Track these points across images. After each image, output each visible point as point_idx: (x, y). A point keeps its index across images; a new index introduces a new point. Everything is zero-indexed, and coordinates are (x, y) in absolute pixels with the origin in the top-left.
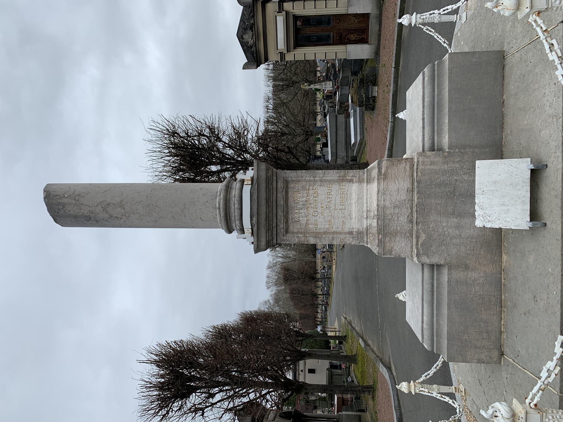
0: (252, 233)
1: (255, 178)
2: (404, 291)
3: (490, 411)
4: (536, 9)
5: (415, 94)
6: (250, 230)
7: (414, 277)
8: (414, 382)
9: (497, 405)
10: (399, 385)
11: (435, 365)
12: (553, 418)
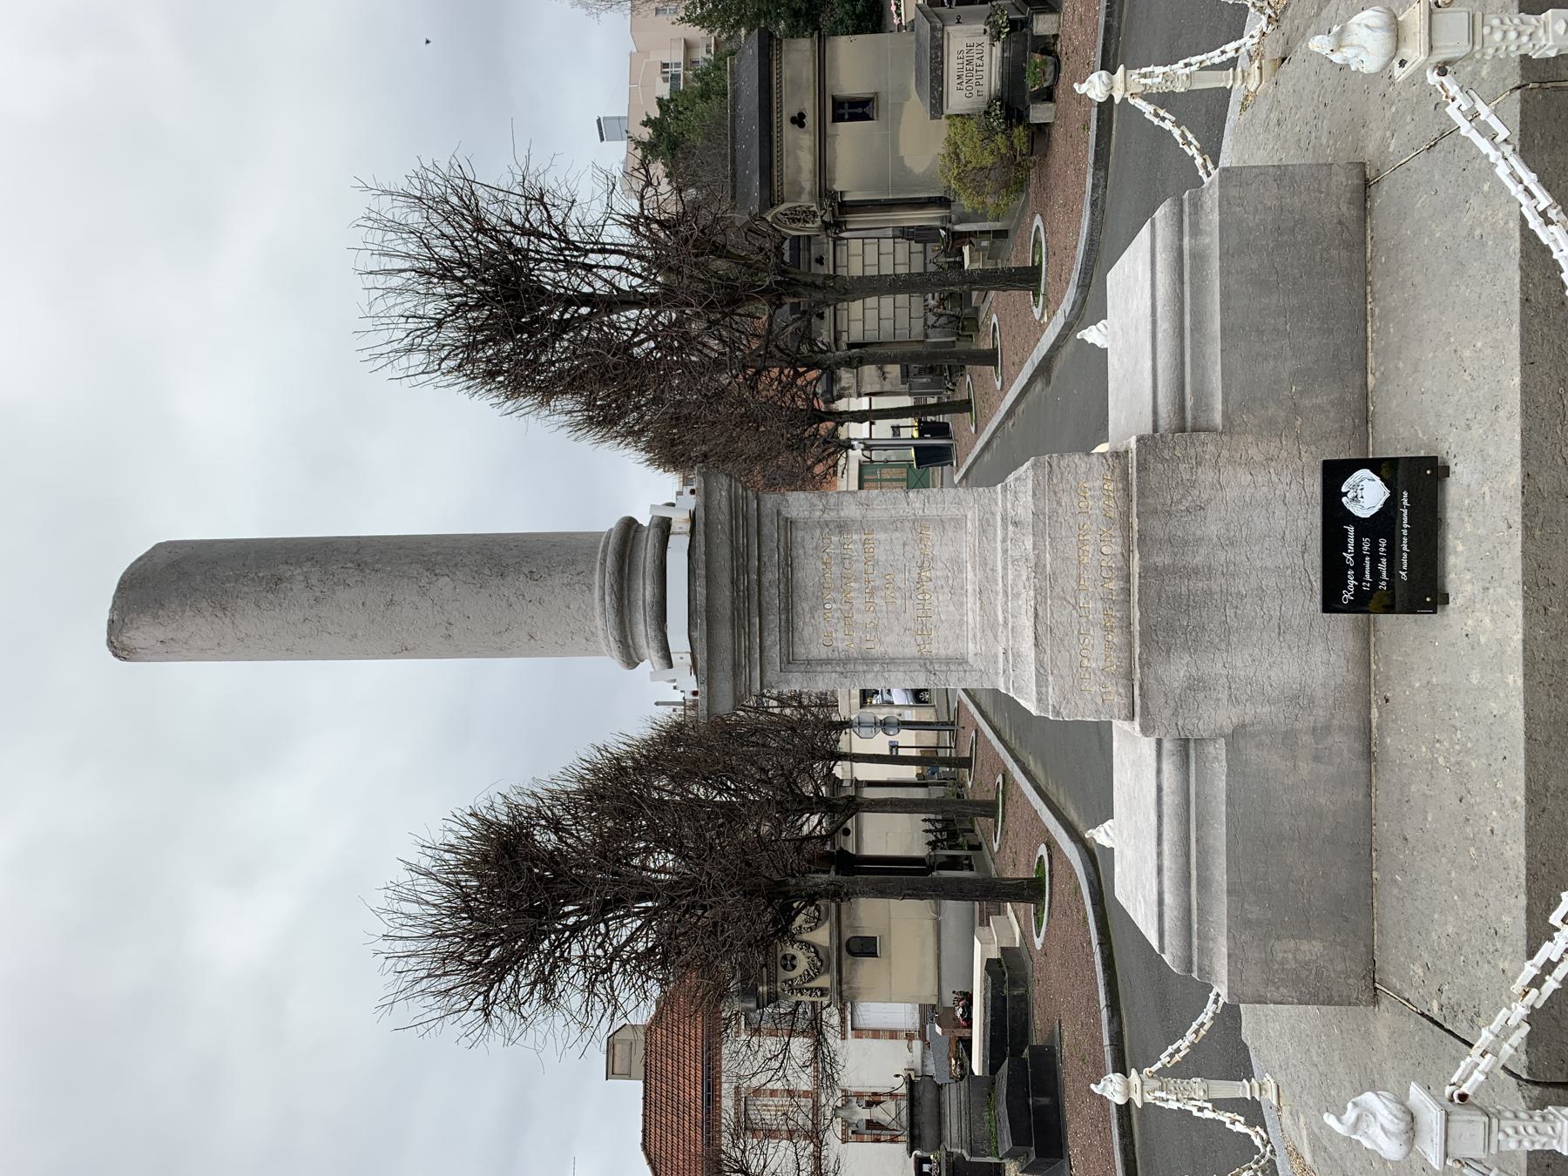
0: (694, 665)
1: (701, 514)
2: (1110, 822)
3: (1351, 1115)
4: (1440, 56)
5: (1135, 279)
6: (688, 659)
7: (1135, 764)
8: (1139, 1072)
9: (1368, 1097)
10: (1098, 1083)
11: (1195, 1026)
12: (1517, 1132)
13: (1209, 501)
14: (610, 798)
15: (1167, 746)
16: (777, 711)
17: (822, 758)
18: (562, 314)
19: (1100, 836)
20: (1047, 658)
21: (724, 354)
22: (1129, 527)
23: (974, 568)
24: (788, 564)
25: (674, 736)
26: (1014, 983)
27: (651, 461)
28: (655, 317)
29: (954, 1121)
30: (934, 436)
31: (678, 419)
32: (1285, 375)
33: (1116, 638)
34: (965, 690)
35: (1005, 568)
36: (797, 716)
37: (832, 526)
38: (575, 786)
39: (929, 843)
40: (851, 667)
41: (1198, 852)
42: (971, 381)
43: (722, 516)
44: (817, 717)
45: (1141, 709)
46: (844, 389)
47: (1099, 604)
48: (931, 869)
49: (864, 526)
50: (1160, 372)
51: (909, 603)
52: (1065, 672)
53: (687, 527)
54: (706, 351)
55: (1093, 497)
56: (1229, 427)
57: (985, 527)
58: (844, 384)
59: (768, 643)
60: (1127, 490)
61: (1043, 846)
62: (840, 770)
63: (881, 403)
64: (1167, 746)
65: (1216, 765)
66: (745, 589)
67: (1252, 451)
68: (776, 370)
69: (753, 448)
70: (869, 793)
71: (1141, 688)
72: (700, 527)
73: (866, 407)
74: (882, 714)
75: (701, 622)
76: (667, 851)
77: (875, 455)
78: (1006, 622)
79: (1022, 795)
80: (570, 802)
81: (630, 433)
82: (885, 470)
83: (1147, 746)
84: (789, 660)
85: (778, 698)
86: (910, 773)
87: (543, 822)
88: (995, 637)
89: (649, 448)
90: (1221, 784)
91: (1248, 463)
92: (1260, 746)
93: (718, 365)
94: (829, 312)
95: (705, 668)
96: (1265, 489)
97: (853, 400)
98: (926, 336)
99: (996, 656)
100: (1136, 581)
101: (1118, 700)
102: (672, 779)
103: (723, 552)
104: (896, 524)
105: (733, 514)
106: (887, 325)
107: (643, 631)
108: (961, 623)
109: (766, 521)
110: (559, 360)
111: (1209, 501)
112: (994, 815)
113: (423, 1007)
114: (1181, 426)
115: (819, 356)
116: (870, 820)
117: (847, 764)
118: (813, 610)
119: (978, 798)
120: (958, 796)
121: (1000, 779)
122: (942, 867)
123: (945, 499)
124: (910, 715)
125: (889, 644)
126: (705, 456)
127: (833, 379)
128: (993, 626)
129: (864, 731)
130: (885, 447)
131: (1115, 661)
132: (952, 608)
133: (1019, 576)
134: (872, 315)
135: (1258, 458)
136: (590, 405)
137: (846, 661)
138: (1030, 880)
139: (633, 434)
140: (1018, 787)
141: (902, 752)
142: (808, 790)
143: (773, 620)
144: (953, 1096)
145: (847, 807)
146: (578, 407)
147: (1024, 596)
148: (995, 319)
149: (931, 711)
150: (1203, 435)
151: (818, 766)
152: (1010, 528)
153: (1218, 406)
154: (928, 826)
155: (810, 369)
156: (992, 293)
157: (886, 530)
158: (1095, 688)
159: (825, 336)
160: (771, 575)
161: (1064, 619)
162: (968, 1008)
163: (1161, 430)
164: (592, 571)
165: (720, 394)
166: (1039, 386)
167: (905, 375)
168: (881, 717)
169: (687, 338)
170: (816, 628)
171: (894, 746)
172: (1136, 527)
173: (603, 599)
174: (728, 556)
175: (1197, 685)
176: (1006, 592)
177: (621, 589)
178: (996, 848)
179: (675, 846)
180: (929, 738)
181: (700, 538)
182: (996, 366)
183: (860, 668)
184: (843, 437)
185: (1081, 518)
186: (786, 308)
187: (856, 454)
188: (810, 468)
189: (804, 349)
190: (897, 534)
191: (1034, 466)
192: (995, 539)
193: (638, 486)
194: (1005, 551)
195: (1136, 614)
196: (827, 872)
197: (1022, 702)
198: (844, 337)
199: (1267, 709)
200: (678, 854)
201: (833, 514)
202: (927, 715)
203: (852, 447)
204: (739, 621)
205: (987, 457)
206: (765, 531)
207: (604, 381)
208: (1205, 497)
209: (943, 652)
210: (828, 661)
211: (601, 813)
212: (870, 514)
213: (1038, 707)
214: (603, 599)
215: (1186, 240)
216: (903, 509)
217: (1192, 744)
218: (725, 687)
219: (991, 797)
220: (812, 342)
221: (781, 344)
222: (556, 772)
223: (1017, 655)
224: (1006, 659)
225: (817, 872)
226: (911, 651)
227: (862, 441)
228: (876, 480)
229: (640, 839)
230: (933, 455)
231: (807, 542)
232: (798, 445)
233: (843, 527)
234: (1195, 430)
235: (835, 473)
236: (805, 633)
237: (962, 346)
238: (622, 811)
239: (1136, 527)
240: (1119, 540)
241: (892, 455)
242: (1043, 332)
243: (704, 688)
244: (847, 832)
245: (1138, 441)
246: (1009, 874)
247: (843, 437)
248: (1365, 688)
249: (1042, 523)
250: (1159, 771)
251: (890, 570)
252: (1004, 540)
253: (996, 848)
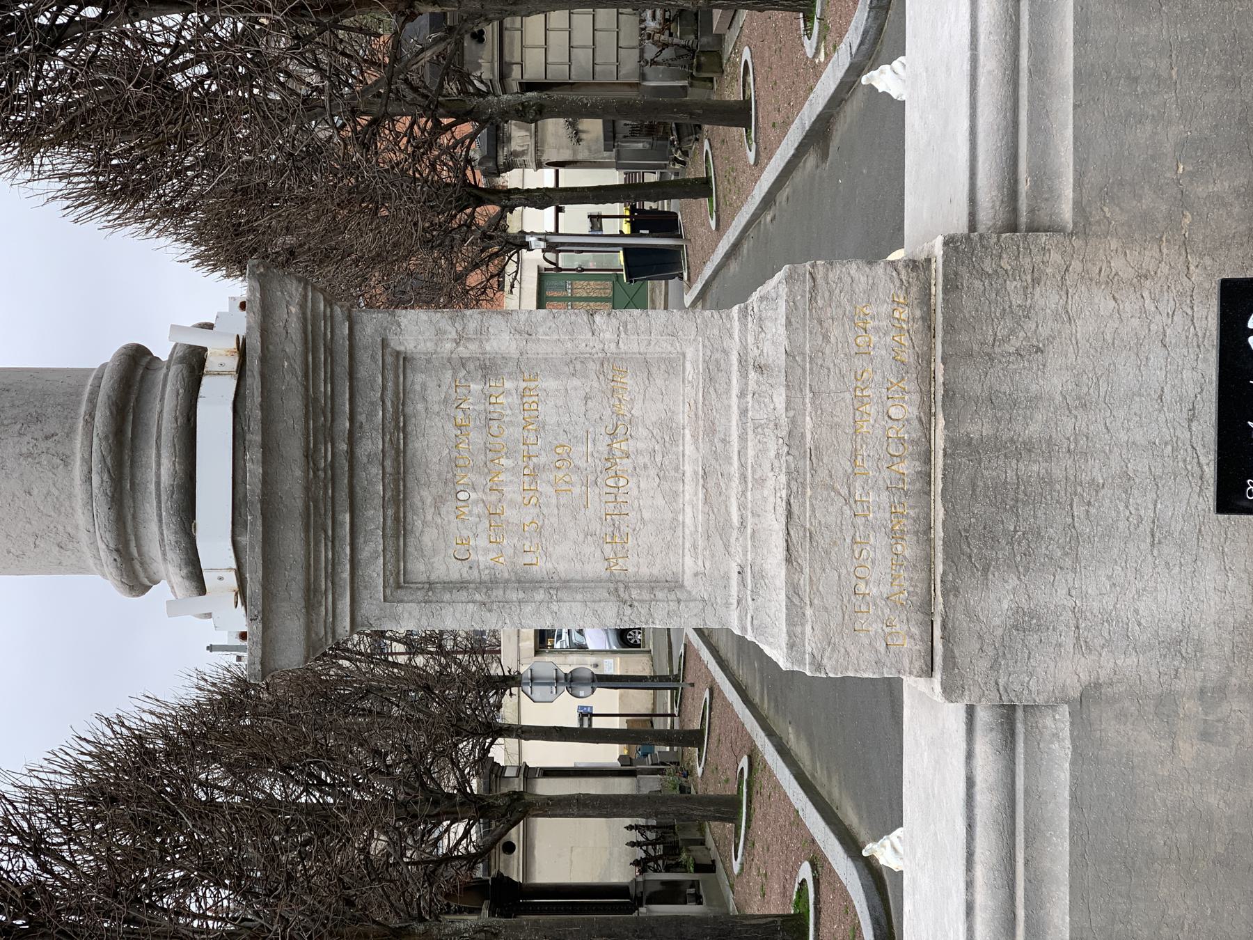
0: (242, 590)
1: (255, 343)
2: (898, 832)
6: (231, 580)
7: (935, 742)
13: (1050, 339)
14: (127, 801)
15: (983, 716)
16: (402, 659)
17: (473, 734)
18: (55, 16)
19: (884, 852)
20: (804, 581)
21: (320, 91)
22: (931, 378)
23: (695, 438)
24: (399, 426)
25: (232, 701)
27: (202, 259)
28: (207, 27)
30: (654, 232)
31: (245, 192)
32: (1168, 147)
33: (908, 549)
34: (699, 632)
35: (743, 438)
36: (434, 668)
37: (471, 366)
38: (69, 781)
39: (636, 863)
40: (498, 593)
41: (1028, 880)
42: (713, 149)
43: (291, 346)
44: (466, 670)
45: (943, 659)
46: (515, 154)
47: (884, 496)
48: (638, 902)
49: (523, 368)
51: (593, 493)
52: (832, 601)
53: (232, 363)
54: (292, 84)
55: (877, 329)
56: (1084, 226)
57: (712, 373)
58: (515, 145)
59: (365, 554)
60: (928, 319)
61: (806, 866)
62: (501, 752)
63: (572, 178)
64: (983, 716)
65: (1055, 746)
66: (324, 465)
67: (1117, 263)
68: (407, 120)
69: (368, 242)
70: (546, 788)
71: (944, 626)
72: (254, 364)
73: (550, 184)
74: (567, 664)
75: (253, 519)
76: (219, 884)
77: (564, 260)
78: (743, 524)
79: (777, 786)
80: (57, 804)
81: (167, 212)
82: (579, 284)
83: (954, 715)
84: (398, 583)
85: (407, 640)
86: (609, 754)
87: (14, 840)
88: (727, 547)
89: (199, 236)
90: (1063, 774)
91: (1112, 282)
92: (1122, 716)
93: (310, 107)
94: (491, 31)
95: (260, 594)
96: (1135, 322)
97: (529, 172)
98: (643, 77)
99: (726, 577)
100: (939, 461)
101: (908, 644)
102: (230, 769)
103: (292, 405)
104: (574, 364)
105: (310, 342)
106: (583, 57)
107: (156, 533)
108: (675, 525)
109: (364, 357)
110: (50, 90)
111: (1050, 339)
112: (733, 817)
114: (1012, 221)
115: (476, 101)
116: (546, 829)
117: (512, 743)
118: (439, 501)
119: (711, 792)
120: (682, 789)
121: (744, 763)
122: (656, 898)
123: (664, 329)
124: (612, 666)
125: (564, 556)
126: (292, 253)
127: (497, 139)
128: (723, 531)
129: (539, 691)
130: (580, 248)
131: (907, 585)
132: (660, 501)
133: (764, 451)
134: (558, 40)
135: (1127, 273)
136: (100, 164)
137: (491, 584)
138: (786, 918)
139: (170, 215)
140: (771, 775)
141: (598, 723)
142: (449, 784)
143: (374, 517)
145: (510, 808)
146: (81, 168)
147: (770, 483)
148: (746, 54)
149: (645, 659)
150: (1043, 237)
151: (465, 746)
152: (752, 375)
153: (1068, 192)
154: (635, 836)
155: (461, 119)
156: (744, 14)
157: (557, 375)
158: (876, 627)
159: (485, 69)
160: (371, 445)
161: (831, 520)
163: (981, 228)
164: (70, 434)
165: (316, 152)
166: (811, 160)
167: (611, 136)
168: (567, 670)
169: (264, 67)
171: (586, 714)
172: (940, 379)
173: (88, 479)
174: (299, 413)
175: (1027, 623)
176: (743, 477)
178: (736, 868)
179: (231, 877)
180: (640, 701)
181: (254, 382)
182: (748, 127)
183: (513, 595)
184: (513, 228)
185: (857, 362)
186: (423, 21)
187: (534, 258)
188: (460, 278)
189: (452, 88)
190: (576, 382)
191: (789, 279)
192: (728, 392)
193: (174, 292)
194: (744, 412)
195: (939, 513)
196: (477, 911)
197: (768, 651)
198: (516, 72)
199: (1132, 660)
200: (235, 888)
201: (473, 347)
202: (637, 665)
203: (527, 246)
204: (317, 520)
205: (734, 267)
206: (362, 372)
207: (122, 126)
208: (1044, 332)
209: (645, 571)
210: (462, 585)
211: (112, 825)
212: (532, 348)
213: (789, 657)
214: (88, 479)
216: (584, 342)
217: (1020, 714)
218: (292, 627)
219: (730, 791)
220: (464, 78)
221: (414, 79)
222: (37, 760)
223: (759, 576)
224: (743, 583)
225: (460, 911)
226: (595, 568)
227: (543, 236)
228: (564, 299)
229: (174, 865)
230: (651, 263)
231: (430, 391)
232: (441, 240)
233: (488, 368)
234: (1033, 228)
235: (501, 286)
236: (426, 539)
237: (696, 94)
238: (146, 822)
239: (940, 379)
240: (916, 398)
241: (589, 260)
242: (818, 76)
243: (258, 628)
244: (509, 848)
245: (946, 243)
246: (755, 908)
247: (513, 228)
249: (801, 369)
250: (970, 756)
251: (563, 439)
252: (742, 394)
253: (736, 868)
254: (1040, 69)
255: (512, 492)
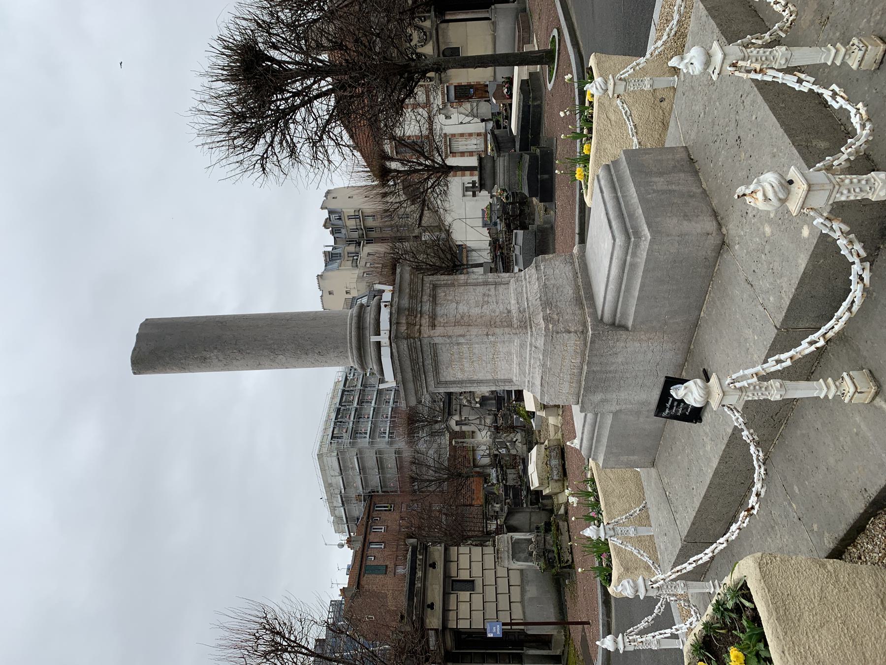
20: (545, 390)
26: (535, 99)
29: (501, 175)
35: (530, 359)
50: (611, 278)
91: (640, 341)
103: (407, 363)
113: (220, 152)
144: (501, 163)
160: (428, 362)
162: (510, 89)
164: (347, 351)
170: (449, 373)
177: (362, 361)
204: (415, 379)
209: (502, 378)
215: (629, 258)
223: (533, 384)
226: (489, 377)
248: (659, 435)
254: (628, 290)
255: (466, 365)
